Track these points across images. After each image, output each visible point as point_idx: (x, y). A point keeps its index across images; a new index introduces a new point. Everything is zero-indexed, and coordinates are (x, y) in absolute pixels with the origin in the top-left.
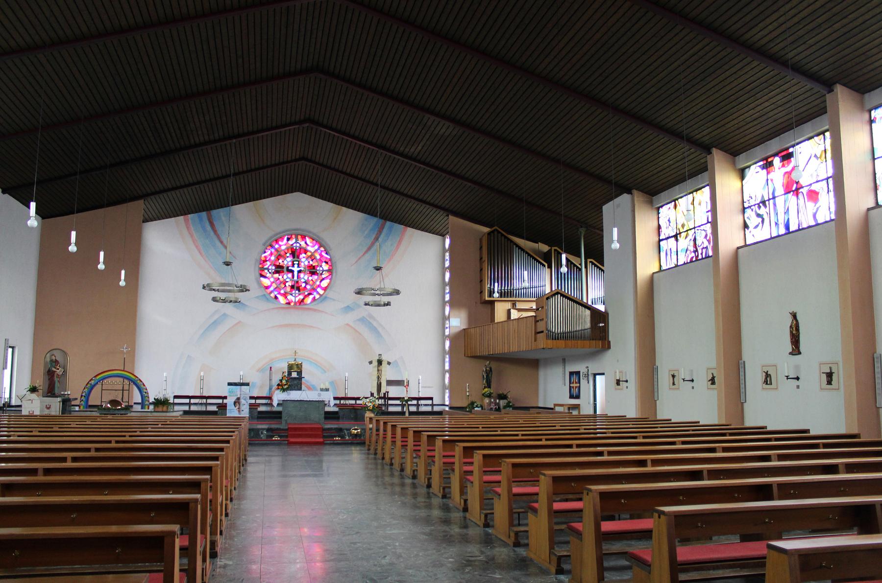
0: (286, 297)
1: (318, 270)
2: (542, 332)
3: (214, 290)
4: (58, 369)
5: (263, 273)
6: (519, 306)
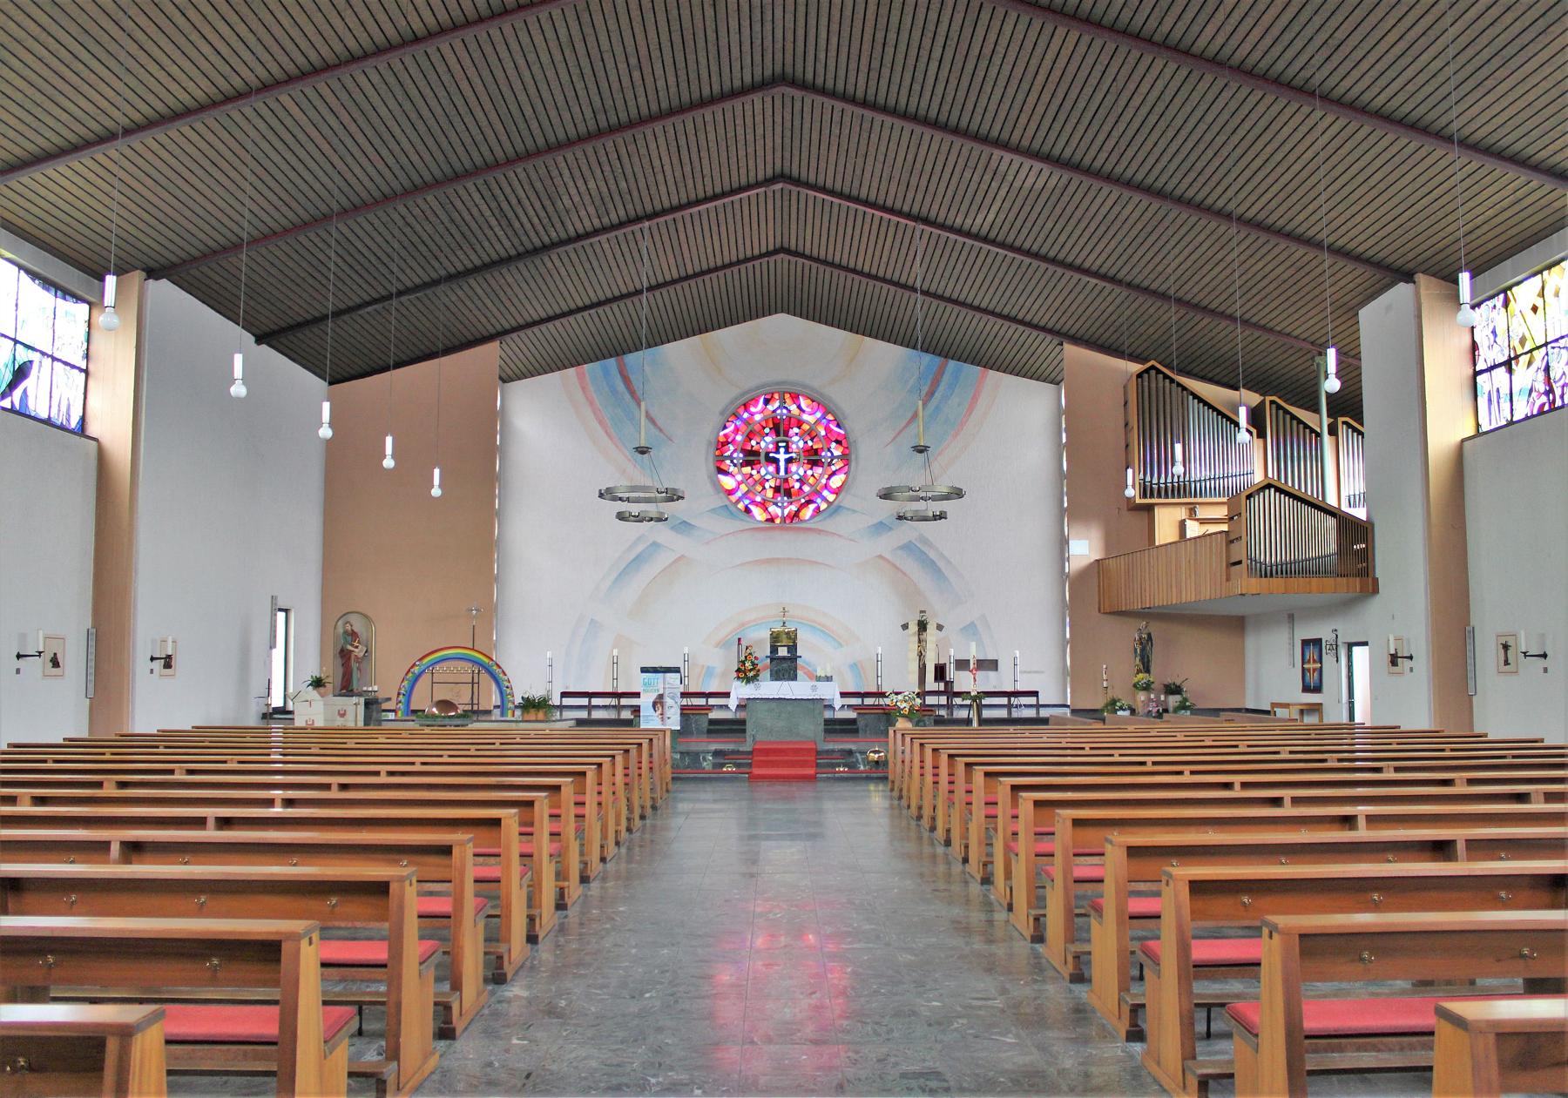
0: (766, 509)
1: (824, 457)
2: (1240, 562)
3: (620, 499)
4: (357, 647)
5: (723, 467)
6: (1202, 513)
